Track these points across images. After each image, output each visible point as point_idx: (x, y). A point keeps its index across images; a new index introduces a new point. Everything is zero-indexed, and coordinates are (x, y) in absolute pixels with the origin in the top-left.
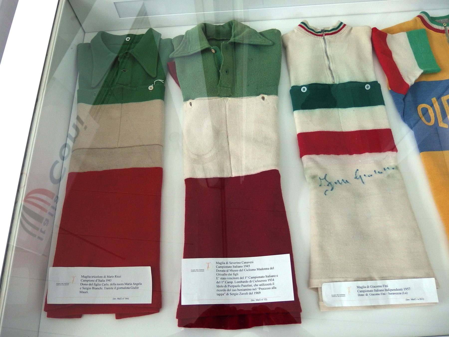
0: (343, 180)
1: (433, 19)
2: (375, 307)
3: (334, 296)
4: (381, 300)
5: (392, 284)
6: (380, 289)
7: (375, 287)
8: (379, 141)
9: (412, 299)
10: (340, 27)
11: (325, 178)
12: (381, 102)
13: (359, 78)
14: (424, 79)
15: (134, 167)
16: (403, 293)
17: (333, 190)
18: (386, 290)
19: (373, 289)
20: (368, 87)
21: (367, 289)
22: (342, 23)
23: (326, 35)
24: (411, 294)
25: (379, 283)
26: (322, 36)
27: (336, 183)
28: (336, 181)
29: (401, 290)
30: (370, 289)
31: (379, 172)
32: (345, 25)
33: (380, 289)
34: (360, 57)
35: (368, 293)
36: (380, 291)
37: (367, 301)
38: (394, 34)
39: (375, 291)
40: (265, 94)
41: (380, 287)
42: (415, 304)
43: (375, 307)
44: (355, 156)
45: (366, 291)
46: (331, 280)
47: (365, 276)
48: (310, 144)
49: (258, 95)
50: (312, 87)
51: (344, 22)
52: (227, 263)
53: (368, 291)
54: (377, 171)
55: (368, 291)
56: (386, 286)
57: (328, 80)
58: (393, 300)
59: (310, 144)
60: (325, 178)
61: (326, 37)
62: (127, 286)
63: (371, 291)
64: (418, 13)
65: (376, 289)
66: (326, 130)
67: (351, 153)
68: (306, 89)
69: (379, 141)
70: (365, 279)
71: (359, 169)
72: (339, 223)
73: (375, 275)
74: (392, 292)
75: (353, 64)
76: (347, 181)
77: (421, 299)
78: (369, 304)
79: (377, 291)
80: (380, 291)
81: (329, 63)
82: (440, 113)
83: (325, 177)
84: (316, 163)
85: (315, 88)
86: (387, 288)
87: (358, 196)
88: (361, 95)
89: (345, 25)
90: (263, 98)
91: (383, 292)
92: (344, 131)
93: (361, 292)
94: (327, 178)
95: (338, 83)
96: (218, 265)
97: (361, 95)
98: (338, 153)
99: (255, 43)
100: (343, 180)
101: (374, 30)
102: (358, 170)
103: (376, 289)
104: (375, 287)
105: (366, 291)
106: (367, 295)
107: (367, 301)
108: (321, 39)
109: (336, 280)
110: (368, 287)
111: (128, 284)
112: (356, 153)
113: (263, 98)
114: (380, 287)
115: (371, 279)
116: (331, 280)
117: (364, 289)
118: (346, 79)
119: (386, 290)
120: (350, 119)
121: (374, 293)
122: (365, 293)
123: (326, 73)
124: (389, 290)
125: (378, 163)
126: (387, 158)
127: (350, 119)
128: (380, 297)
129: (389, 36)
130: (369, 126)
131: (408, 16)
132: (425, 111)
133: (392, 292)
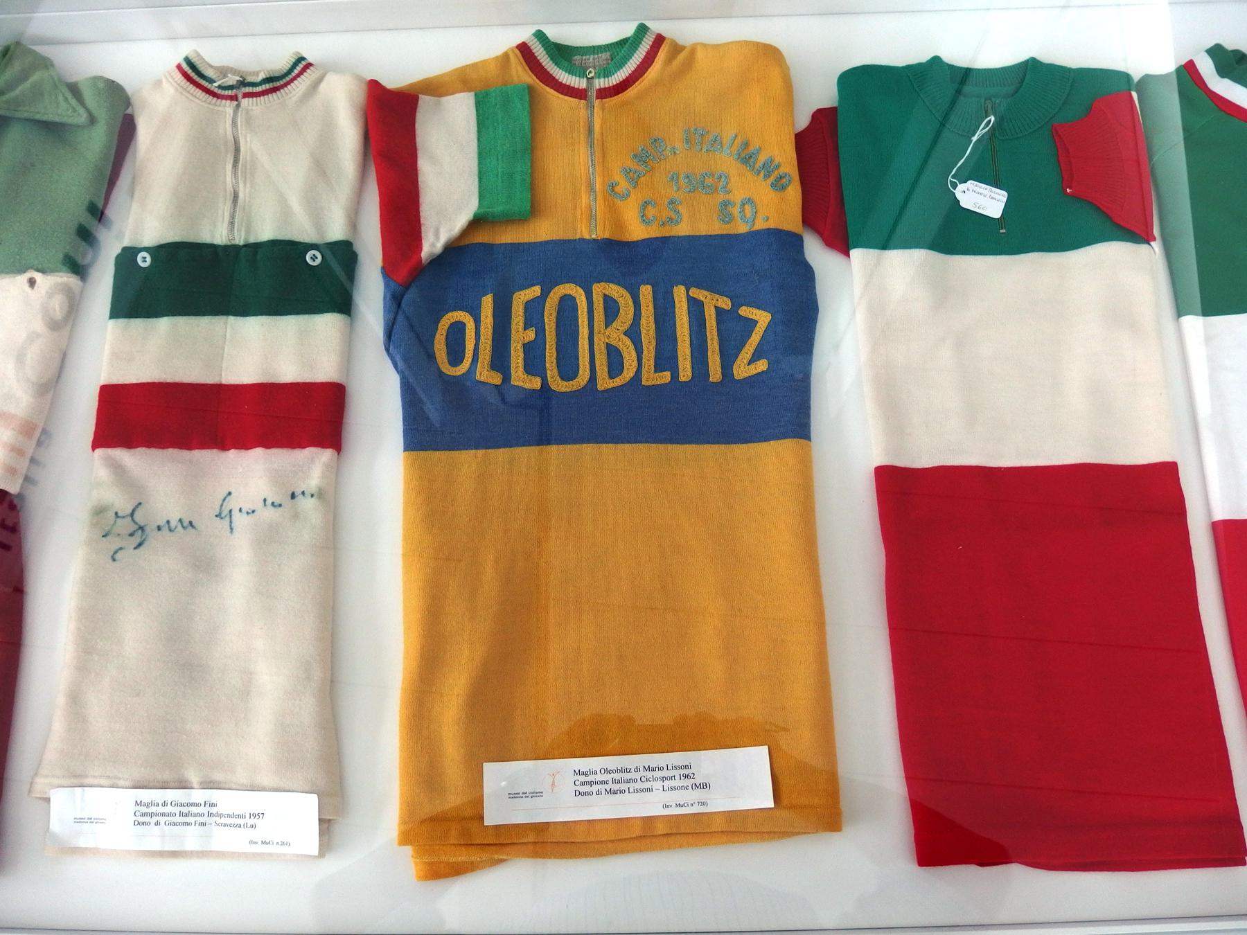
0: (180, 520)
1: (562, 53)
2: (174, 854)
3: (80, 820)
4: (191, 838)
5: (226, 801)
6: (194, 810)
7: (182, 805)
8: (308, 416)
9: (264, 843)
10: (301, 65)
11: (132, 514)
12: (343, 304)
13: (302, 230)
14: (482, 237)
15: (278, 318)
16: (246, 826)
17: (142, 548)
18: (210, 815)
19: (176, 810)
20: (314, 258)
21: (160, 809)
22: (302, 59)
23: (246, 95)
24: (264, 830)
25: (198, 795)
26: (233, 98)
27: (159, 528)
28: (162, 522)
29: (242, 816)
30: (168, 809)
31: (273, 504)
32: (309, 65)
33: (194, 810)
34: (321, 168)
35: (162, 820)
36: (196, 815)
37: (153, 839)
38: (441, 95)
39: (181, 814)
40: (38, 270)
41: (198, 805)
42: (271, 855)
43: (174, 854)
44: (232, 453)
45: (156, 815)
46: (76, 781)
47: (167, 776)
48: (137, 417)
49: (22, 270)
50: (168, 253)
51: (310, 59)
52: (165, 804)
53: (163, 814)
54: (269, 502)
55: (163, 814)
56: (212, 805)
57: (217, 233)
58: (223, 839)
59: (137, 417)
60: (132, 514)
61: (245, 102)
62: (649, 774)
63: (170, 815)
64: (524, 34)
65: (185, 810)
66: (169, 380)
67: (224, 447)
68: (149, 259)
69: (308, 416)
70: (164, 786)
71: (233, 491)
72: (135, 632)
73: (193, 776)
74: (224, 820)
75: (303, 187)
76: (191, 523)
77: (283, 844)
78: (157, 846)
79: (185, 815)
80: (196, 815)
81: (237, 183)
82: (490, 342)
83: (134, 510)
84: (118, 470)
85: (176, 256)
86: (213, 810)
87: (205, 566)
88: (294, 279)
89: (309, 65)
90: (32, 282)
91: (201, 820)
92: (224, 382)
93: (144, 816)
94: (137, 517)
95: (242, 243)
96: (139, 808)
97: (294, 279)
98: (186, 443)
99: (45, 118)
100: (180, 520)
101: (374, 87)
102: (230, 494)
103: (185, 810)
104: (182, 805)
105: (156, 815)
106: (157, 824)
107: (153, 839)
108: (228, 106)
109: (96, 782)
110: (165, 804)
111: (654, 770)
112: (236, 448)
113: (32, 282)
114: (198, 805)
115: (183, 785)
116: (76, 781)
117: (153, 809)
118: (265, 232)
119: (210, 815)
120: (258, 349)
121: (178, 819)
122: (155, 819)
123: (220, 212)
124: (216, 815)
125: (277, 478)
126: (311, 464)
127: (258, 349)
128: (193, 831)
129: (425, 101)
130: (289, 372)
131: (489, 43)
132: (457, 330)
133: (224, 820)
